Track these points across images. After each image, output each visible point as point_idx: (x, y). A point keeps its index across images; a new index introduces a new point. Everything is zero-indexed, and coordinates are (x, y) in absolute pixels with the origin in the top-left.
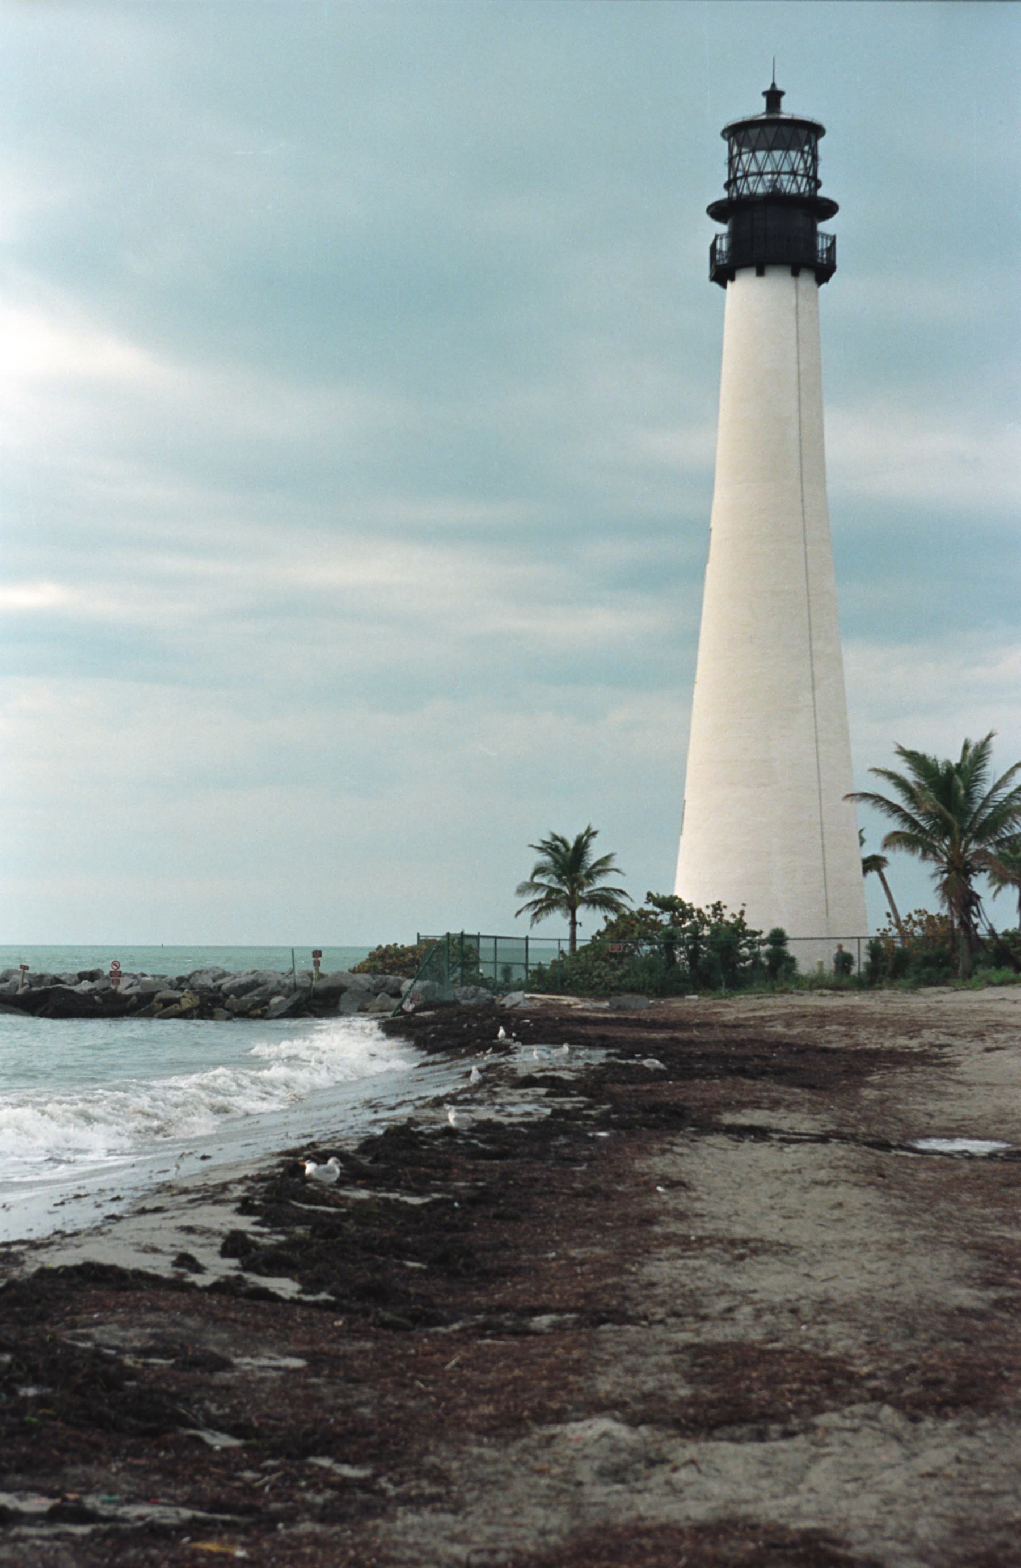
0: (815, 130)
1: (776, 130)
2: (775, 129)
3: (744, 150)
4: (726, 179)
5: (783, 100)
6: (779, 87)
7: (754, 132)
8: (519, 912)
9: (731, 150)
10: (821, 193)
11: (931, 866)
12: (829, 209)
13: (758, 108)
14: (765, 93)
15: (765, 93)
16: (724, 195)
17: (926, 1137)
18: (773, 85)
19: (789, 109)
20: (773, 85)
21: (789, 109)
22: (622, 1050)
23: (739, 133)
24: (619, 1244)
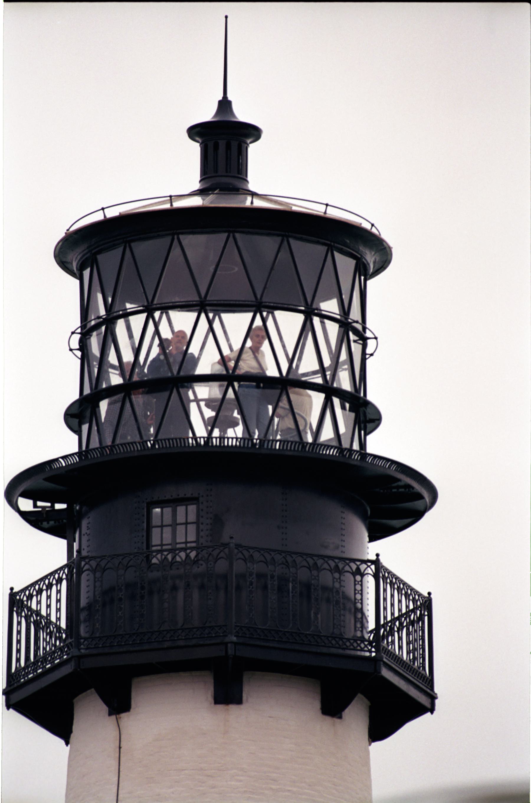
0: (356, 247)
1: (221, 240)
5: (255, 151)
6: (242, 113)
10: (378, 444)
13: (175, 177)
14: (197, 132)
15: (197, 132)
16: (64, 444)
18: (225, 105)
20: (225, 105)
21: (274, 177)
23: (111, 255)
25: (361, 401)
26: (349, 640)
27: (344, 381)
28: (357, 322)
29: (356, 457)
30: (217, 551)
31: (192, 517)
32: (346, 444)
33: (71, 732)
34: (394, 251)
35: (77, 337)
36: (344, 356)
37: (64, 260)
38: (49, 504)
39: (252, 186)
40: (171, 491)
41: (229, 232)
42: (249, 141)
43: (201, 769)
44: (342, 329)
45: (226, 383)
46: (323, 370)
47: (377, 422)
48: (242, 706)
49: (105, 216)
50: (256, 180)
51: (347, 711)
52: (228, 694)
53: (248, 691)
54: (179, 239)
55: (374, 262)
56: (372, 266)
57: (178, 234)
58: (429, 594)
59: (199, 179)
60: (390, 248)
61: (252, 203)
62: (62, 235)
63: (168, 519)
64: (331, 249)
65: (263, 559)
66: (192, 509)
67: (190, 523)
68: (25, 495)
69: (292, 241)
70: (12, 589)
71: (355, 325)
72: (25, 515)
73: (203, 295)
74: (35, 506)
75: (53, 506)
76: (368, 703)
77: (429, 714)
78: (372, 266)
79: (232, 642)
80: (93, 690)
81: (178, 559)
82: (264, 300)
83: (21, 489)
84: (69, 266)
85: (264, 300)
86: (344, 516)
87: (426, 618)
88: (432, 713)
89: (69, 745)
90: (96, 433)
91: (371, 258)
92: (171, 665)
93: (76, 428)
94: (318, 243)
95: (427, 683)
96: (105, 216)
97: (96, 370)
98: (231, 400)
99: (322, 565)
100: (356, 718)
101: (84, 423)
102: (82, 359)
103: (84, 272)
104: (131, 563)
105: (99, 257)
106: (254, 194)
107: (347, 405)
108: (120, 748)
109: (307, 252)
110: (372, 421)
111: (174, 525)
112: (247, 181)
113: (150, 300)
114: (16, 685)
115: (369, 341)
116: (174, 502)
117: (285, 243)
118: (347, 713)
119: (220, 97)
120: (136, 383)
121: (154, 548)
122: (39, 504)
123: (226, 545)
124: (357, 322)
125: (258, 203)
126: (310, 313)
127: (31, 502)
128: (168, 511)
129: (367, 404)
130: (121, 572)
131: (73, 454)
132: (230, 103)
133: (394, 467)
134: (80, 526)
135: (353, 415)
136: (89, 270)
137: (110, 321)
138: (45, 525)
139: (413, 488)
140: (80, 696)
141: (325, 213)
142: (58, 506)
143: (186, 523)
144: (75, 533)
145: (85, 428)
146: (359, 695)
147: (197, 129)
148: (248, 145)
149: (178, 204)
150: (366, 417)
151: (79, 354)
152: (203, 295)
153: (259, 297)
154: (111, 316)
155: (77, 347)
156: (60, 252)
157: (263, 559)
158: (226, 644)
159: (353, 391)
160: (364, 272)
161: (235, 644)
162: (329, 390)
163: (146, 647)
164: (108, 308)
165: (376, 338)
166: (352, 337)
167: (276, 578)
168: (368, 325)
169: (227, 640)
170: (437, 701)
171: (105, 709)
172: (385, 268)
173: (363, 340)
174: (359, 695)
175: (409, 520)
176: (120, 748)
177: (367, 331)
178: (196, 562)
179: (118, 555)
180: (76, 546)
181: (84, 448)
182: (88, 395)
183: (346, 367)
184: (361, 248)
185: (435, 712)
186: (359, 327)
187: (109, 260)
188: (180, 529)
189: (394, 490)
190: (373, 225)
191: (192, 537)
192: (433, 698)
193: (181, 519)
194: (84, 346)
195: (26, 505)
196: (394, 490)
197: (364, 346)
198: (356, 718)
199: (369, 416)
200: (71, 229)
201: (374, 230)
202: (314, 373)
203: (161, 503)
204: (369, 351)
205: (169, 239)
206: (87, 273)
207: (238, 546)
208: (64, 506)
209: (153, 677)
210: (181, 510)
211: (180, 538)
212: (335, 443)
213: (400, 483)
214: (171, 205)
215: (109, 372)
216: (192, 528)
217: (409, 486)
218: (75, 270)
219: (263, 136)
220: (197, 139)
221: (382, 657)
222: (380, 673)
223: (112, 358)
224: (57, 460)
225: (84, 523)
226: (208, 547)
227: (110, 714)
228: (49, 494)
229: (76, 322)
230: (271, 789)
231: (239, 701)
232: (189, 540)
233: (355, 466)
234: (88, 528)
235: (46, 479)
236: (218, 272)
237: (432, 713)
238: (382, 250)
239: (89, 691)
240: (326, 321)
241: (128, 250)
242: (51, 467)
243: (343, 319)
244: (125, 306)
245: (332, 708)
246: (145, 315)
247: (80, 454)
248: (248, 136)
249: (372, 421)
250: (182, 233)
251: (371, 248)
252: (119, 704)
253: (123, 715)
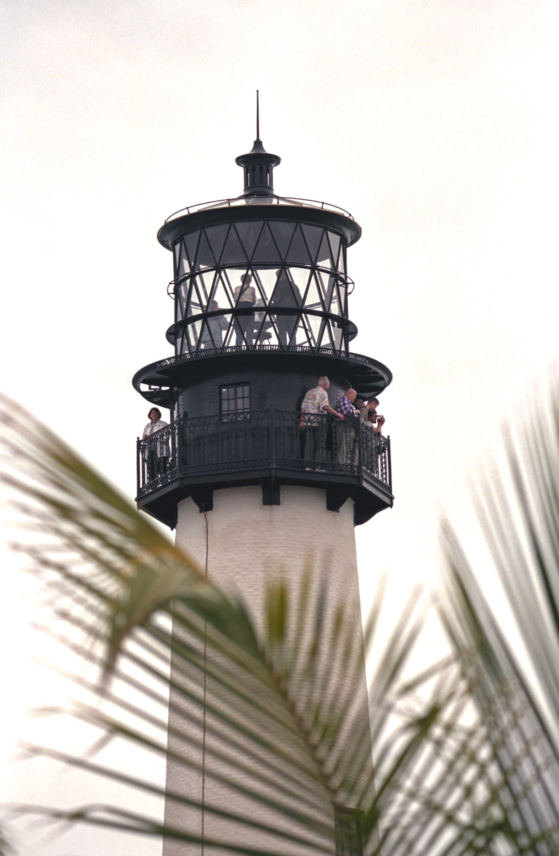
0: (342, 228)
1: (259, 226)
2: (222, 229)
3: (307, 345)
5: (276, 170)
6: (269, 149)
7: (215, 233)
8: (36, 751)
9: (177, 270)
10: (356, 347)
13: (228, 187)
14: (240, 160)
15: (240, 160)
16: (166, 351)
18: (258, 144)
20: (258, 144)
21: (288, 185)
23: (193, 237)
25: (346, 322)
26: (343, 465)
27: (335, 309)
28: (342, 274)
29: (343, 355)
30: (263, 414)
31: (247, 394)
32: (337, 348)
33: (177, 522)
34: (362, 230)
35: (172, 286)
36: (335, 294)
37: (163, 239)
38: (158, 387)
39: (275, 193)
40: (232, 378)
41: (265, 220)
42: (273, 165)
43: (257, 543)
44: (333, 279)
45: (264, 313)
46: (322, 302)
47: (355, 334)
48: (280, 506)
49: (189, 212)
50: (277, 190)
51: (342, 508)
52: (271, 499)
53: (283, 496)
54: (234, 225)
55: (351, 237)
56: (349, 239)
57: (234, 222)
58: (389, 437)
59: (243, 189)
60: (360, 228)
61: (278, 202)
62: (162, 224)
63: (232, 395)
64: (326, 230)
65: (290, 418)
66: (247, 388)
67: (246, 397)
68: (145, 382)
69: (303, 225)
70: (138, 438)
71: (341, 275)
72: (144, 394)
73: (250, 259)
74: (150, 388)
75: (160, 388)
76: (354, 503)
77: (389, 508)
78: (349, 239)
79: (273, 468)
80: (190, 498)
81: (239, 419)
82: (287, 261)
83: (142, 378)
84: (166, 243)
85: (287, 261)
86: (337, 391)
87: (387, 451)
88: (391, 507)
89: (174, 530)
90: (186, 345)
91: (349, 234)
92: (236, 482)
93: (173, 341)
94: (318, 226)
95: (388, 489)
96: (189, 212)
97: (185, 306)
98: (268, 322)
99: (313, 419)
100: (347, 511)
101: (178, 338)
102: (176, 300)
103: (176, 247)
104: (211, 422)
105: (185, 237)
106: (278, 198)
107: (336, 324)
108: (207, 531)
109: (311, 231)
110: (352, 333)
111: (236, 398)
112: (273, 190)
113: (217, 262)
114: (143, 496)
115: (349, 285)
116: (235, 385)
117: (298, 227)
118: (342, 509)
119: (255, 139)
120: (210, 313)
121: (224, 413)
122: (152, 387)
123: (268, 410)
124: (342, 274)
125: (282, 203)
126: (314, 269)
127: (147, 386)
128: (232, 390)
129: (350, 323)
130: (205, 427)
131: (172, 357)
132: (261, 142)
133: (367, 361)
134: (178, 400)
135: (341, 330)
136: (179, 245)
137: (192, 276)
138: (155, 400)
139: (378, 373)
140: (181, 502)
141: (322, 208)
142: (164, 388)
143: (243, 398)
144: (175, 404)
145: (179, 341)
146: (349, 498)
147: (241, 159)
148: (272, 168)
149: (233, 204)
150: (349, 331)
151: (173, 296)
152: (250, 259)
153: (283, 259)
154: (194, 273)
155: (172, 292)
156: (161, 234)
157: (290, 418)
158: (270, 469)
159: (340, 315)
160: (345, 244)
161: (276, 469)
162: (326, 316)
163: (221, 472)
164: (192, 268)
165: (353, 283)
166: (340, 283)
167: (299, 430)
168: (348, 275)
169: (271, 467)
170: (394, 501)
171: (197, 508)
172: (357, 241)
173: (346, 284)
174: (349, 498)
175: (375, 393)
176: (207, 531)
177: (348, 279)
178: (250, 420)
179: (203, 417)
180: (175, 412)
181: (179, 354)
182: (180, 321)
183: (336, 300)
184: (344, 229)
185: (393, 507)
186: (343, 276)
187: (192, 239)
188: (240, 401)
189: (367, 375)
190: (350, 215)
191: (247, 406)
192: (392, 498)
193: (240, 394)
194: (177, 292)
195: (144, 387)
196: (367, 375)
197: (346, 288)
198: (347, 511)
199: (350, 331)
200: (168, 221)
201: (351, 218)
202: (317, 304)
203: (225, 386)
204: (349, 291)
205: (228, 225)
206: (178, 247)
207: (276, 411)
208: (167, 388)
209: (226, 490)
210: (240, 389)
211: (240, 406)
212: (330, 347)
213: (371, 371)
214: (229, 205)
215: (191, 307)
216: (247, 401)
217: (376, 373)
218: (170, 245)
219: (282, 162)
220: (242, 164)
221: (363, 475)
222: (362, 484)
223: (194, 298)
224: (164, 360)
225: (181, 398)
226: (258, 411)
227: (201, 512)
228: (157, 380)
229: (172, 278)
230: (300, 555)
231: (278, 503)
232: (245, 407)
233: (344, 361)
234: (183, 401)
235: (157, 372)
236: (258, 245)
237: (391, 507)
238: (355, 230)
239: (187, 499)
240: (321, 273)
241: (203, 233)
242: (160, 364)
243: (333, 272)
244: (199, 267)
245: (333, 506)
246: (214, 272)
247: (176, 357)
248: (272, 162)
249: (352, 333)
250: (236, 222)
251: (349, 229)
252: (206, 506)
253: (209, 512)
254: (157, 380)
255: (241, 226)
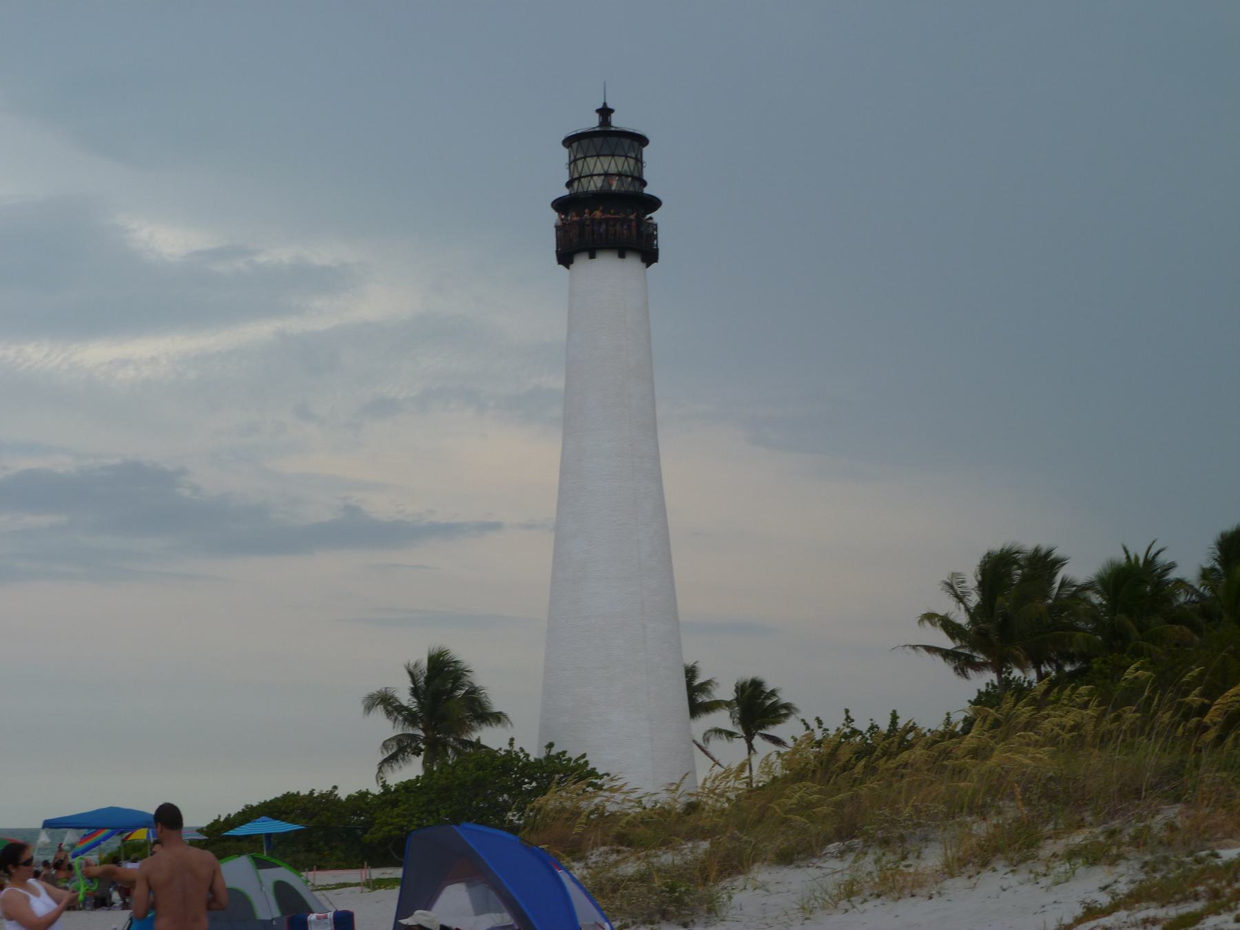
0: (642, 141)
1: (606, 139)
4: (567, 179)
6: (610, 106)
10: (647, 190)
11: (229, 885)
12: (654, 203)
13: (593, 122)
14: (598, 111)
15: (598, 111)
16: (565, 192)
17: (283, 837)
19: (617, 122)
21: (617, 122)
22: (454, 767)
24: (1125, 716)
34: (249, 803)
52: (592, 256)
92: (579, 251)
150: (644, 184)
187: (575, 145)
219: (996, 546)
228: (560, 205)
254: (560, 205)
255: (596, 140)
